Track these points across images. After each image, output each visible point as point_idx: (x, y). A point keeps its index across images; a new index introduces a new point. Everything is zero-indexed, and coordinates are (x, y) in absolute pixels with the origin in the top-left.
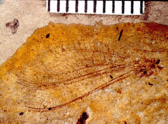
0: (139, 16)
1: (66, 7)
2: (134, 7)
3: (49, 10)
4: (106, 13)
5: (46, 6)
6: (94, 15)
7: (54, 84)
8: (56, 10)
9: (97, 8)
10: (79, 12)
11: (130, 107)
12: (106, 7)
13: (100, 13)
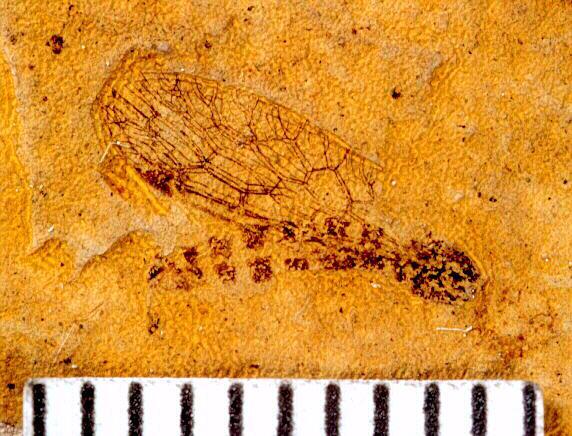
0: (394, 376)
2: (80, 422)
3: (529, 392)
4: (226, 383)
5: (547, 408)
7: (229, 220)
8: (98, 393)
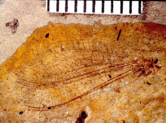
0: (137, 16)
1: (66, 7)
2: (132, 7)
3: (48, 10)
4: (105, 13)
5: (45, 6)
6: (93, 15)
7: (53, 83)
8: (56, 10)
9: (96, 8)
10: (78, 12)
11: (128, 107)
12: (105, 7)
13: (99, 12)
